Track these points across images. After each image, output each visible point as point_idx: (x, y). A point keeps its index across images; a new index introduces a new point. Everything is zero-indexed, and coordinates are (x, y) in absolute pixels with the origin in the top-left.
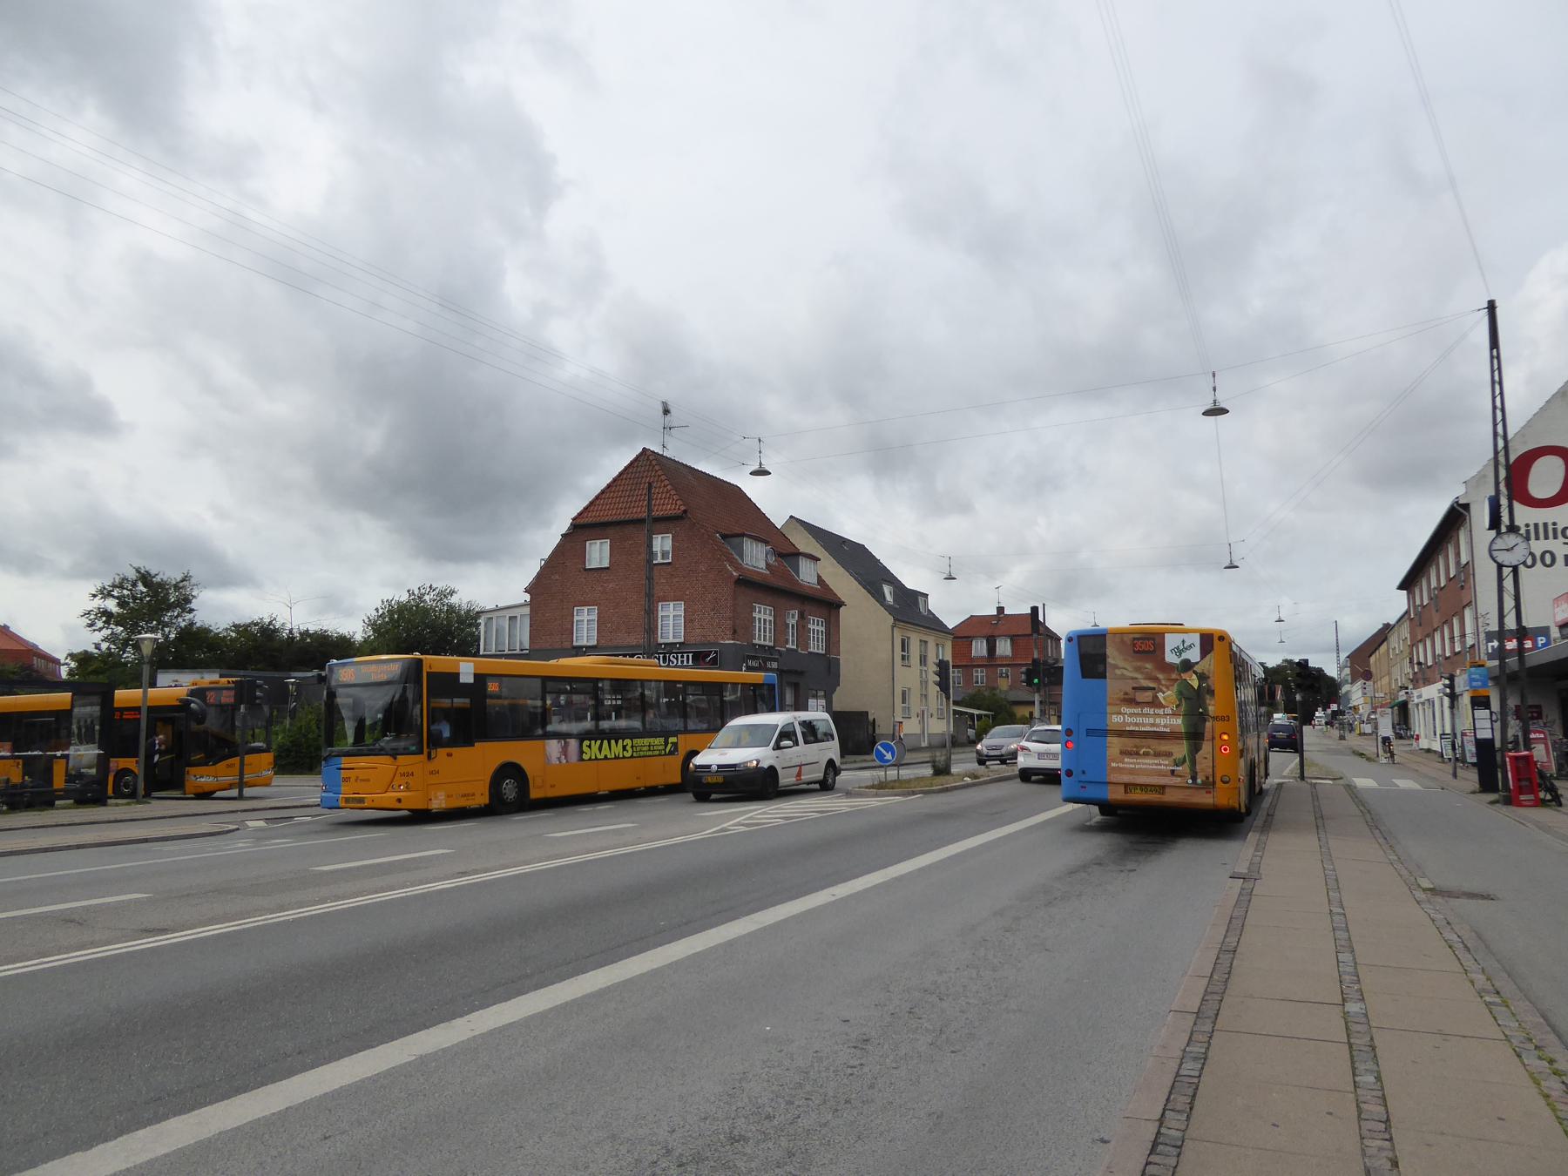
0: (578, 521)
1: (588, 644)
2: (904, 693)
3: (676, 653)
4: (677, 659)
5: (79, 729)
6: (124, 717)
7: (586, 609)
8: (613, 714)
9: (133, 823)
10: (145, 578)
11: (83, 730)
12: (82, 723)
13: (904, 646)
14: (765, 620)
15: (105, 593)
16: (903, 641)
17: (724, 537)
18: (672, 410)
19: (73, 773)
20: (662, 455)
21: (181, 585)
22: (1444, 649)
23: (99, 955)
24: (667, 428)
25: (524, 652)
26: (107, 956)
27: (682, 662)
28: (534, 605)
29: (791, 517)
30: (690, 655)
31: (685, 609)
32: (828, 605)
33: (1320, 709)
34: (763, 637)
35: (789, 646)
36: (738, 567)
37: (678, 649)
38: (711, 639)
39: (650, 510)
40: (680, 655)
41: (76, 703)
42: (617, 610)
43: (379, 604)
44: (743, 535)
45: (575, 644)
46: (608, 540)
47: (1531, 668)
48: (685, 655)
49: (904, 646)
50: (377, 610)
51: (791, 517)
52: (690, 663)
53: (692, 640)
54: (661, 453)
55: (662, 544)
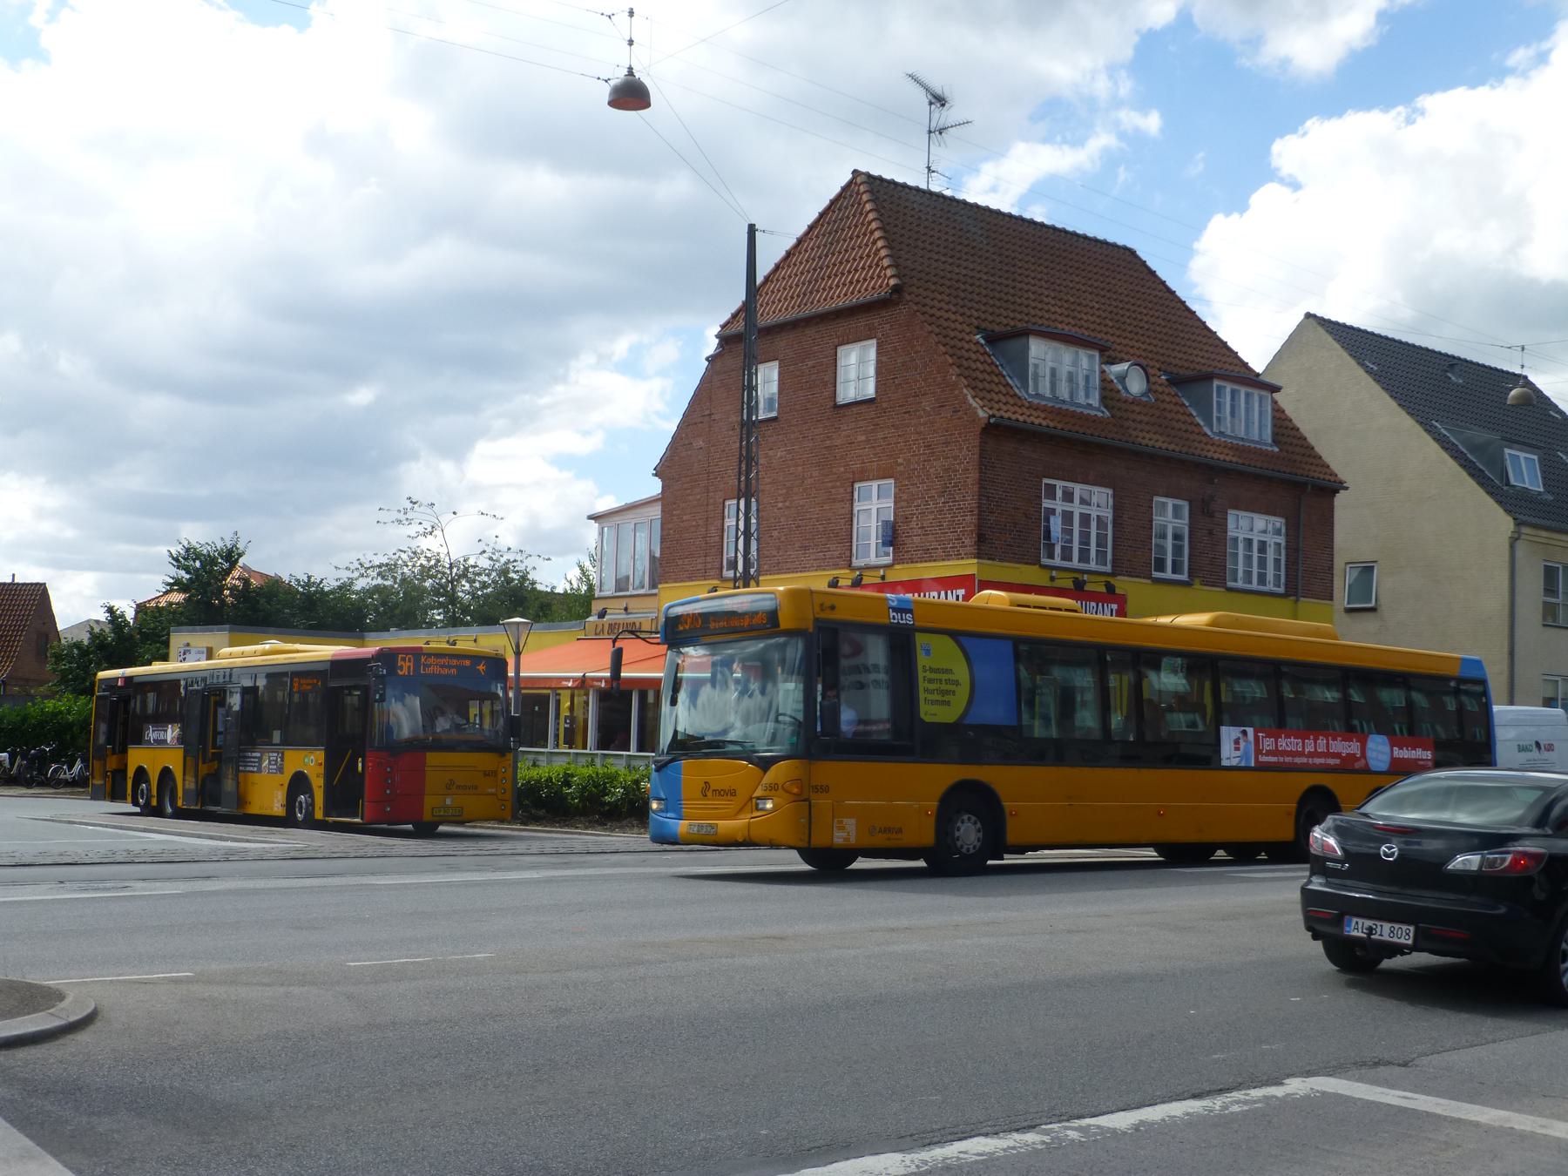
0: (728, 332)
6: (376, 704)
8: (350, 751)
14: (1085, 519)
17: (992, 339)
18: (947, 94)
22: (1086, 604)
24: (937, 131)
28: (666, 499)
29: (1308, 316)
42: (787, 504)
47: (815, 849)
51: (1308, 316)
54: (923, 186)
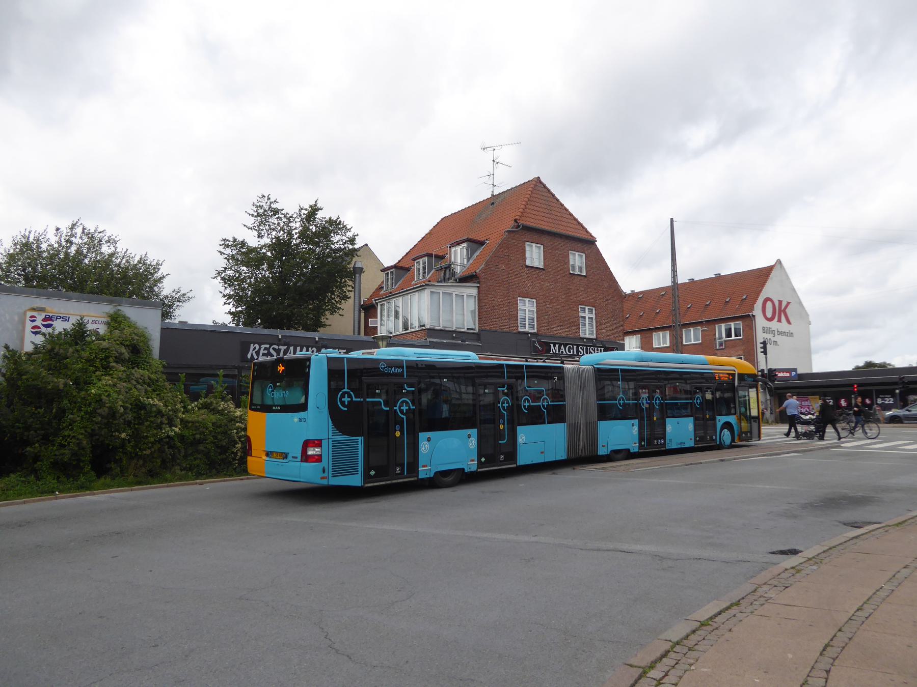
3: (573, 345)
4: (583, 350)
30: (602, 349)
31: (537, 306)
37: (584, 342)
38: (612, 338)
40: (596, 348)
42: (551, 306)
48: (599, 349)
53: (602, 338)
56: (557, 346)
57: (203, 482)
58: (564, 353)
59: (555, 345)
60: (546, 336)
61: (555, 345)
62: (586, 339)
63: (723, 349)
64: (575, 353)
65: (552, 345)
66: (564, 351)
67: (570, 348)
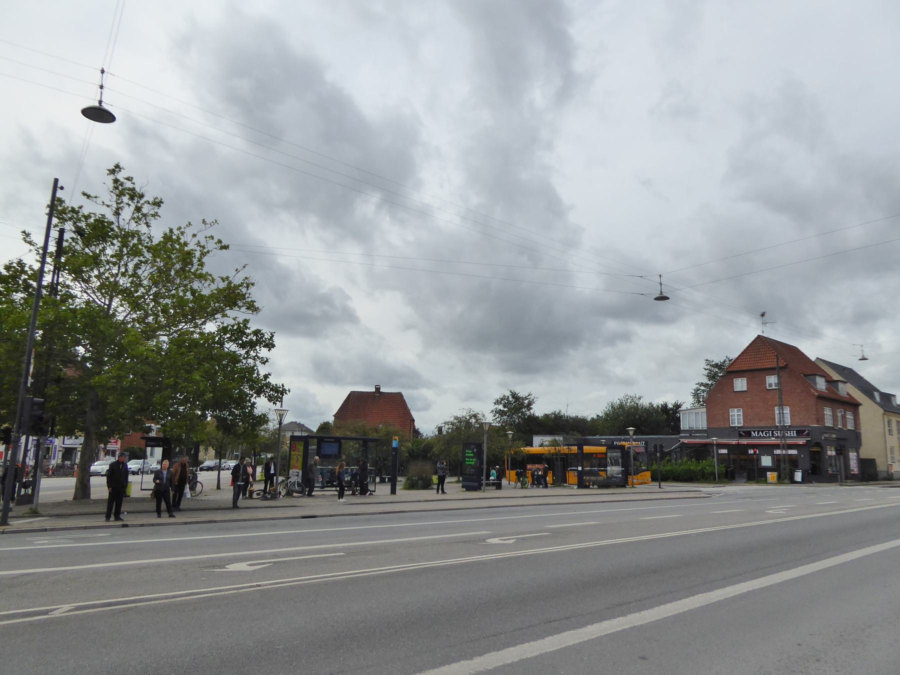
1: (738, 426)
2: (891, 449)
5: (611, 461)
7: (736, 409)
9: (525, 498)
10: (514, 395)
11: (613, 461)
12: (612, 459)
13: (889, 422)
15: (497, 402)
16: (889, 421)
17: (805, 376)
19: (610, 476)
20: (571, 454)
21: (529, 397)
23: (498, 557)
25: (704, 429)
26: (417, 569)
27: (791, 435)
30: (795, 431)
31: (790, 410)
32: (854, 406)
33: (165, 346)
34: (829, 423)
35: (840, 427)
36: (817, 391)
39: (778, 364)
40: (789, 431)
41: (608, 452)
43: (606, 405)
44: (815, 375)
45: (731, 425)
46: (745, 378)
48: (792, 432)
49: (889, 422)
50: (606, 408)
52: (795, 435)
53: (795, 425)
54: (762, 335)
55: (772, 380)
56: (756, 432)
57: (220, 559)
58: (762, 436)
59: (754, 432)
60: (748, 428)
61: (754, 432)
62: (694, 430)
63: (130, 435)
64: (771, 435)
65: (752, 432)
66: (761, 434)
67: (766, 433)
